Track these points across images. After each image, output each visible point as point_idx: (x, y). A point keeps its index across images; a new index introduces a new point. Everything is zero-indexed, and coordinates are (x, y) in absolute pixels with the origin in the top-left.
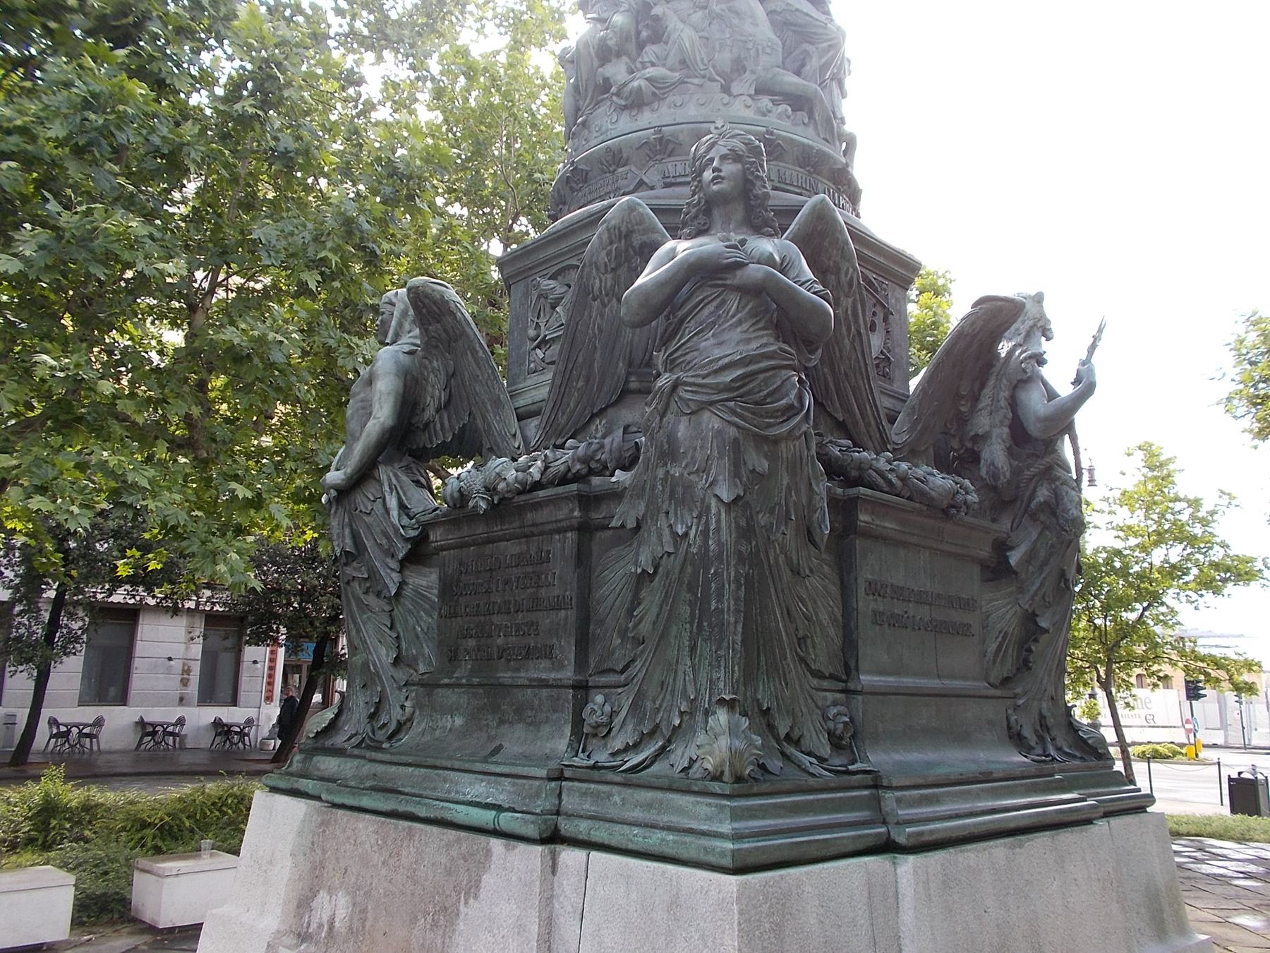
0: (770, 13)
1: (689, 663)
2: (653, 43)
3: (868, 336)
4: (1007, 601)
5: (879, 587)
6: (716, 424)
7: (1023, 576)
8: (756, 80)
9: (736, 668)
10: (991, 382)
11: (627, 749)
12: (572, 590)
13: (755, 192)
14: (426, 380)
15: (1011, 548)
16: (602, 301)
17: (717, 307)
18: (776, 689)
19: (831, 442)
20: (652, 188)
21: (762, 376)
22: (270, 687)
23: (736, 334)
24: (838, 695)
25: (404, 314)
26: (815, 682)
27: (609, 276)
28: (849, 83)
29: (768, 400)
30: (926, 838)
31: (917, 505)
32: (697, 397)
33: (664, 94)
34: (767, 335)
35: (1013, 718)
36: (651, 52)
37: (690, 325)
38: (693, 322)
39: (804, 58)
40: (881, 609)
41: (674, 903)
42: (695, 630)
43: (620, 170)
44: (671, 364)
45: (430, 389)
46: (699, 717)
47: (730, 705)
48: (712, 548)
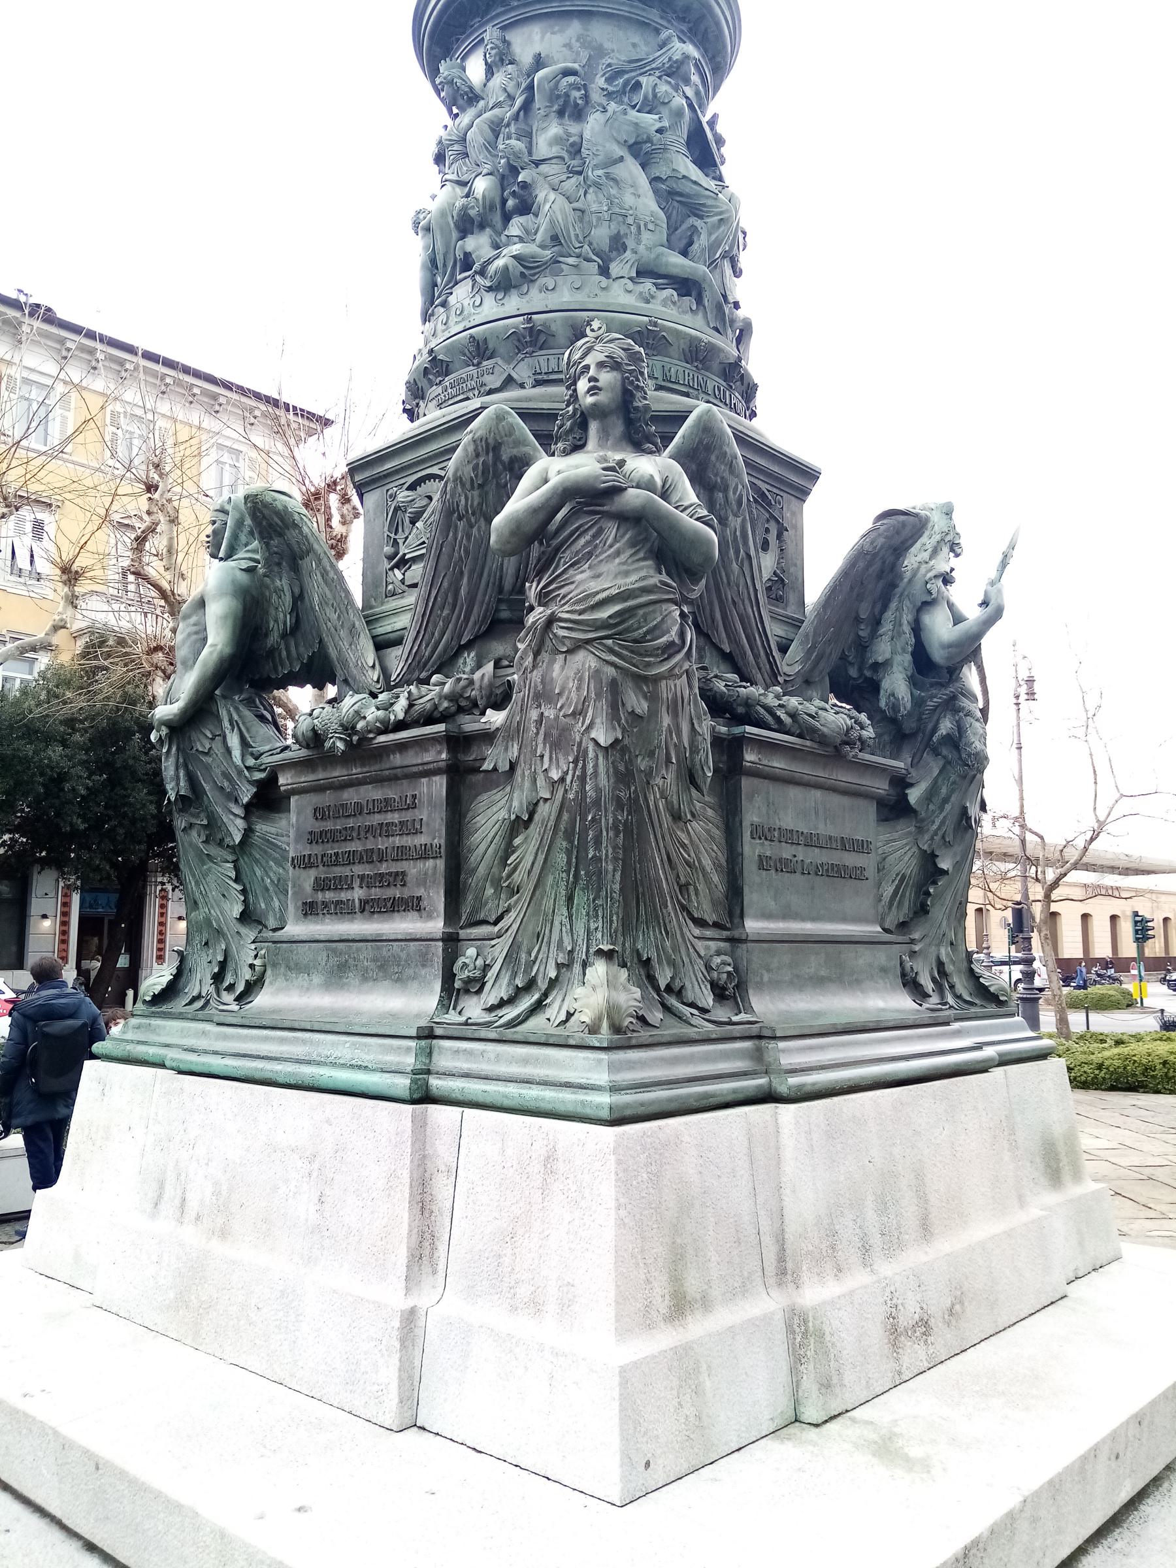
0: (655, 180)
1: (566, 913)
2: (521, 215)
3: (758, 558)
4: (904, 842)
5: (766, 830)
6: (592, 662)
7: (923, 814)
8: (638, 260)
9: (615, 918)
10: (893, 605)
11: (502, 1004)
12: (440, 837)
13: (635, 404)
14: (269, 601)
15: (911, 785)
16: (469, 521)
17: (595, 537)
18: (656, 938)
19: (716, 676)
20: (522, 386)
21: (641, 612)
22: (64, 946)
23: (614, 566)
24: (722, 944)
25: (239, 524)
26: (697, 932)
27: (476, 493)
28: (745, 260)
29: (648, 637)
30: (808, 1089)
31: (808, 743)
32: (574, 635)
33: (534, 275)
34: (648, 567)
35: (908, 965)
36: (515, 227)
37: (565, 555)
38: (568, 552)
39: (691, 236)
40: (768, 854)
41: (549, 1159)
42: (571, 879)
43: (485, 363)
44: (544, 598)
45: (272, 612)
46: (577, 968)
47: (608, 955)
48: (589, 794)
